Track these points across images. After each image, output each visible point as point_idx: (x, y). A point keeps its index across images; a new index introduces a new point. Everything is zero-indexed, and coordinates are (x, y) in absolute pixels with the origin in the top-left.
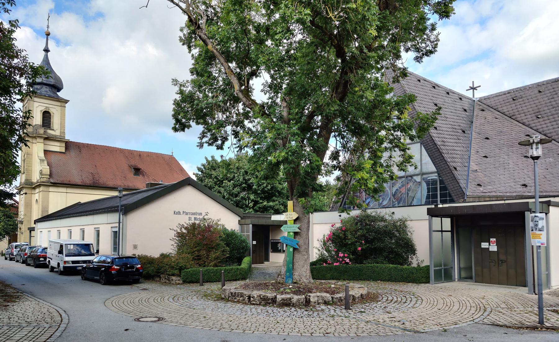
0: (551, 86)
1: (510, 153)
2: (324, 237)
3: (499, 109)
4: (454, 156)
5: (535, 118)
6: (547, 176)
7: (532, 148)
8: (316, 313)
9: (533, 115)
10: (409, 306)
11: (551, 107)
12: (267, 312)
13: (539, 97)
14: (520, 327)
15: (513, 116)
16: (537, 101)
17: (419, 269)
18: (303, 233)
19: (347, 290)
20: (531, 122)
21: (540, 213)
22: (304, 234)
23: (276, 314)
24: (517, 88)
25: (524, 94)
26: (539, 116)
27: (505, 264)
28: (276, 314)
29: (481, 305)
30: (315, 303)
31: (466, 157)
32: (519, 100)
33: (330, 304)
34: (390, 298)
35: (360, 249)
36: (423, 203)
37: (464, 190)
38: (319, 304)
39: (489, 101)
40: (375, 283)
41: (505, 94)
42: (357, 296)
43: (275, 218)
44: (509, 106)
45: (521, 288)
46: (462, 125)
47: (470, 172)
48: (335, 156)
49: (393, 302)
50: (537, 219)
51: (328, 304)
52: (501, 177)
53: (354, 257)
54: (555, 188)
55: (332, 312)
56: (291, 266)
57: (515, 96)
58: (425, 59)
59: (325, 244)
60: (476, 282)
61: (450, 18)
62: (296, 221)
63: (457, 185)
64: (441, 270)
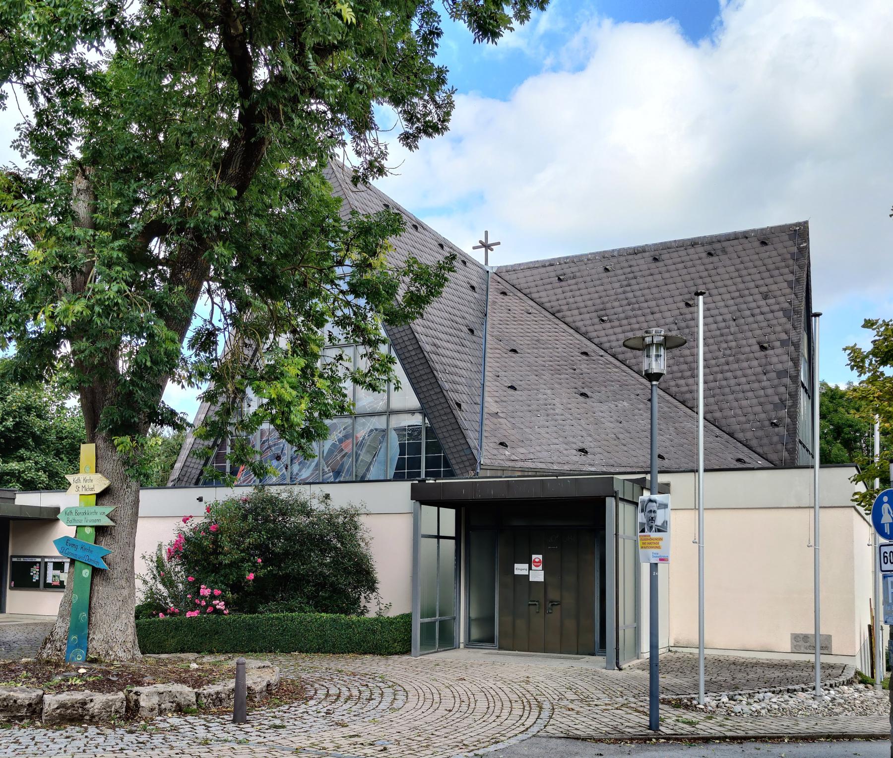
0: (627, 261)
1: (556, 386)
2: (160, 549)
3: (534, 296)
4: (456, 379)
5: (597, 320)
6: (620, 436)
7: (648, 356)
8: (157, 739)
9: (595, 314)
10: (382, 706)
11: (625, 302)
12: (17, 742)
13: (606, 280)
14: (619, 739)
15: (559, 311)
16: (601, 288)
17: (380, 622)
18: (120, 529)
19: (239, 673)
20: (590, 329)
21: (660, 493)
22: (121, 533)
23: (44, 748)
24: (567, 258)
25: (579, 271)
26: (605, 318)
27: (557, 609)
28: (44, 748)
29: (528, 696)
30: (152, 710)
31: (478, 384)
32: (570, 282)
33: (192, 713)
34: (333, 691)
35: (251, 576)
36: (391, 475)
37: (475, 452)
38: (161, 712)
39: (515, 276)
40: (288, 656)
41: (544, 266)
42: (258, 688)
43: (26, 499)
44: (552, 292)
45: (588, 658)
46: (466, 315)
47: (485, 416)
48: (206, 340)
49: (342, 699)
50: (653, 506)
51: (186, 713)
52: (542, 431)
53: (236, 596)
54: (635, 460)
55: (201, 732)
56: (82, 621)
57: (562, 272)
58: (423, 141)
59: (160, 565)
60: (500, 648)
61: (500, 40)
62: (101, 497)
63: (463, 441)
64: (434, 623)
